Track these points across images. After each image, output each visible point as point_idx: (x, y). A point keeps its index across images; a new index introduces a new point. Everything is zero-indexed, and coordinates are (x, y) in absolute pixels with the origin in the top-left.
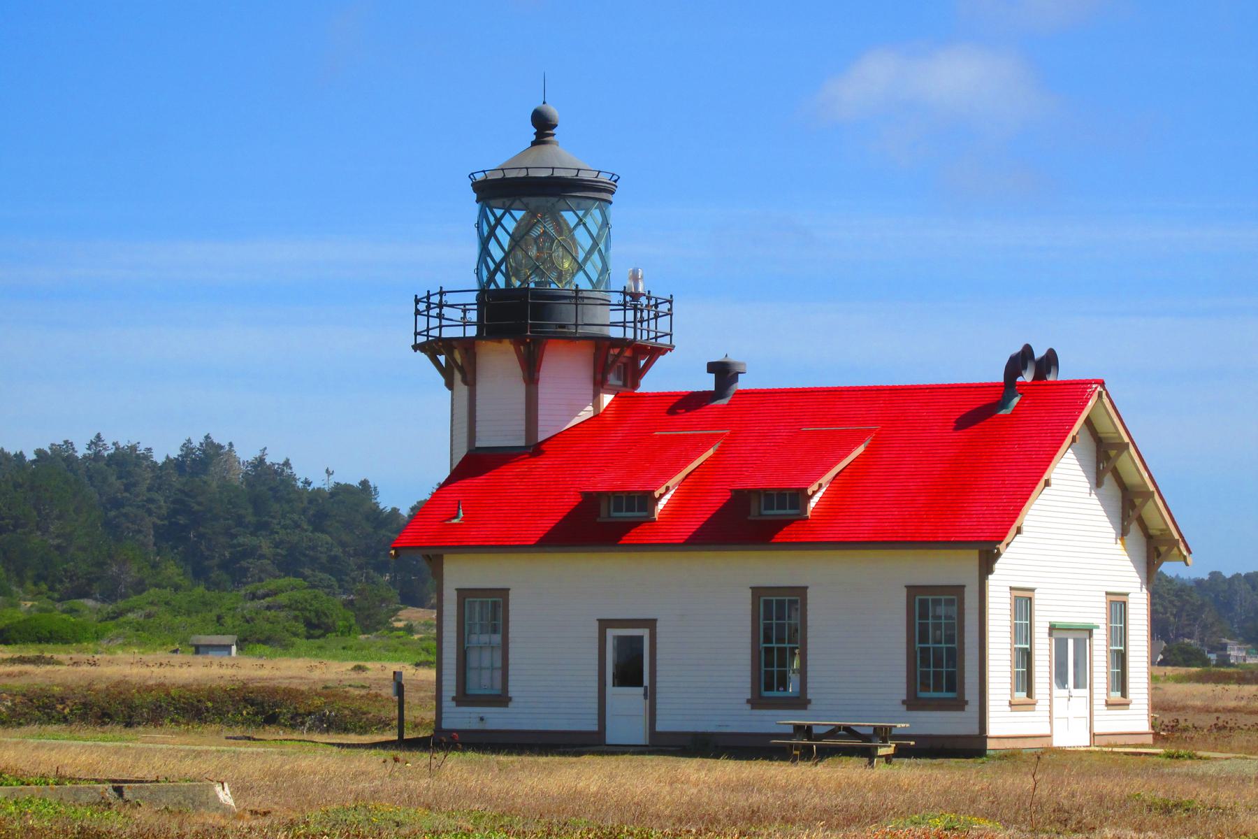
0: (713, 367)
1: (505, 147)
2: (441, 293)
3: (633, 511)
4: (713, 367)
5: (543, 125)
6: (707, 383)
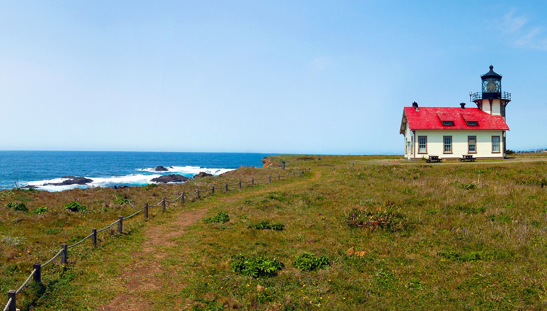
0: (461, 104)
1: (487, 71)
4: (461, 104)
5: (491, 68)
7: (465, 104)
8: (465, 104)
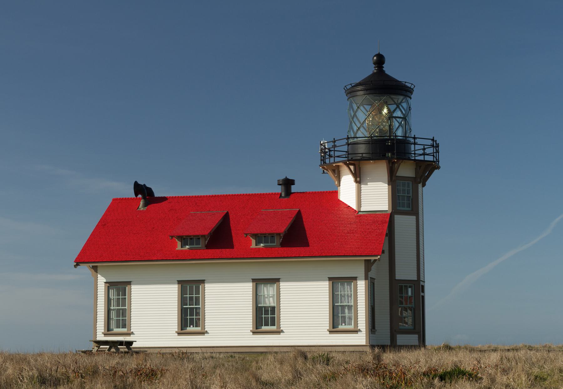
2: (334, 142)
3: (193, 245)
5: (380, 61)
6: (279, 189)
7: (292, 182)
8: (292, 182)
